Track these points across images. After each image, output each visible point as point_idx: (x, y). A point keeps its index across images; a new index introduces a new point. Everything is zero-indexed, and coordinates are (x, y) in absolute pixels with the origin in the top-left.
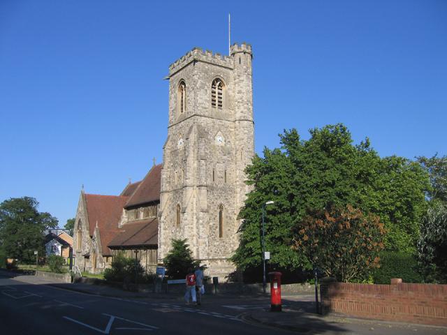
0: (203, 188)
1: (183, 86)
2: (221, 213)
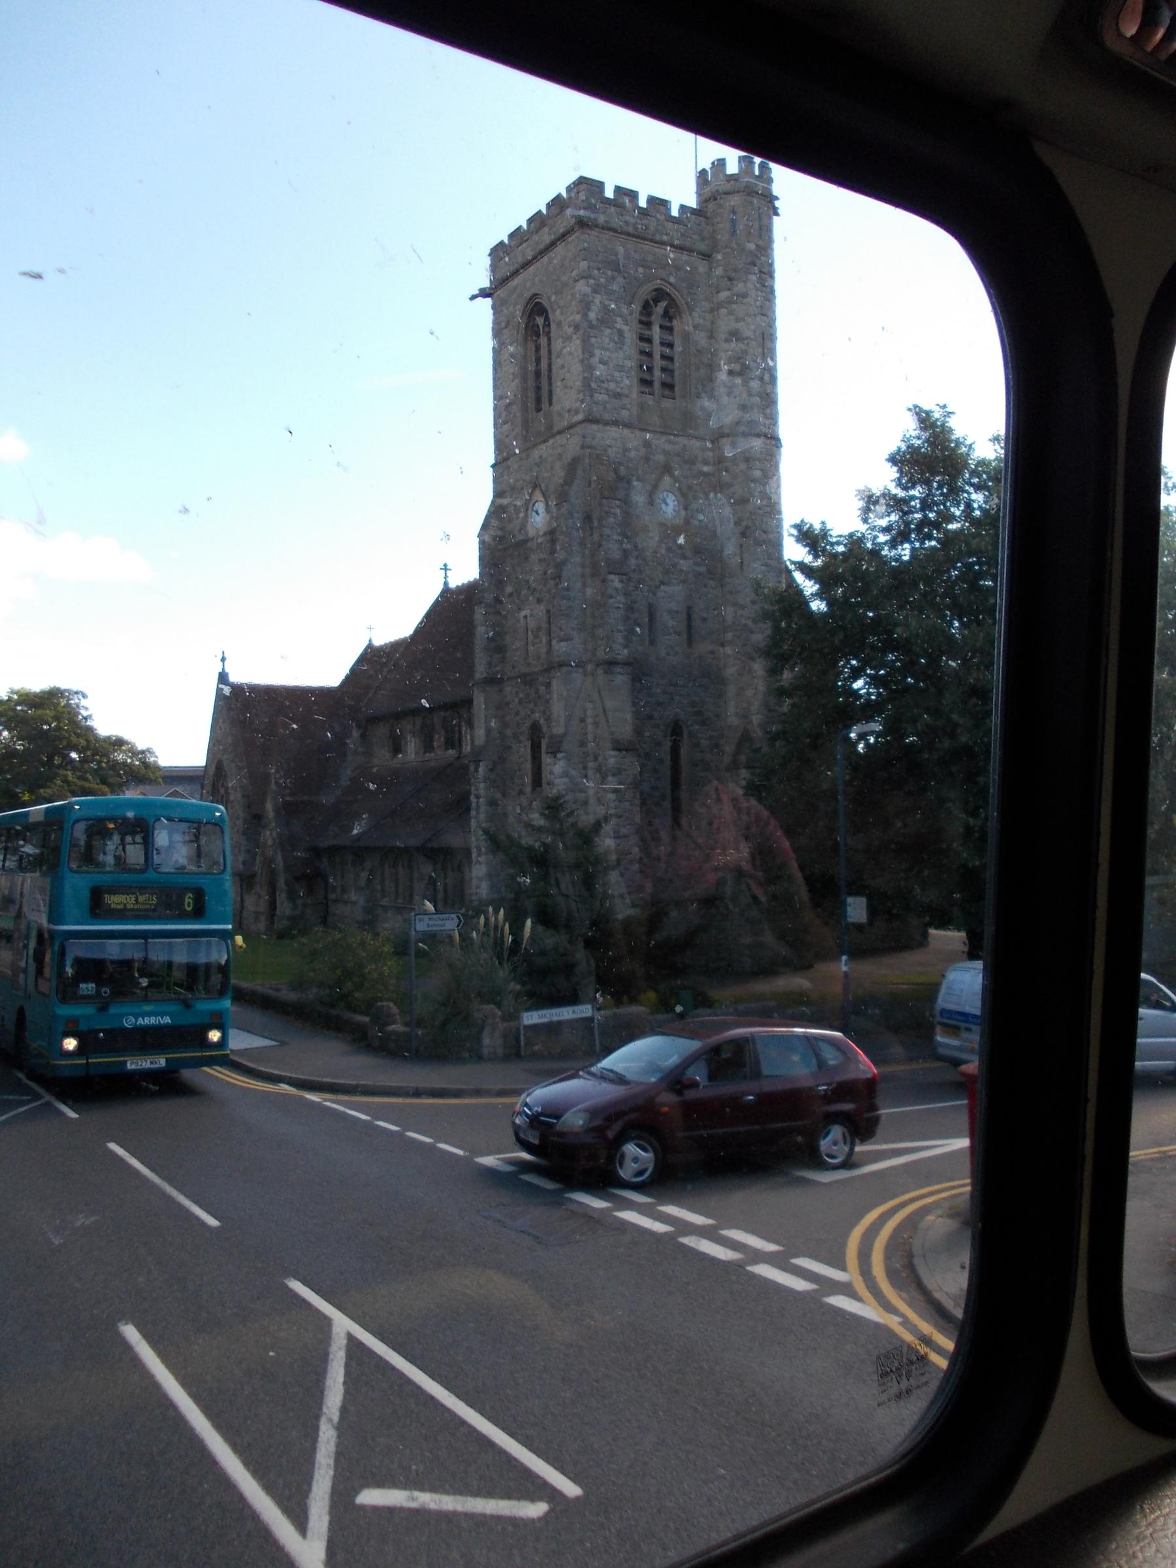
0: (618, 669)
1: (540, 321)
2: (675, 751)
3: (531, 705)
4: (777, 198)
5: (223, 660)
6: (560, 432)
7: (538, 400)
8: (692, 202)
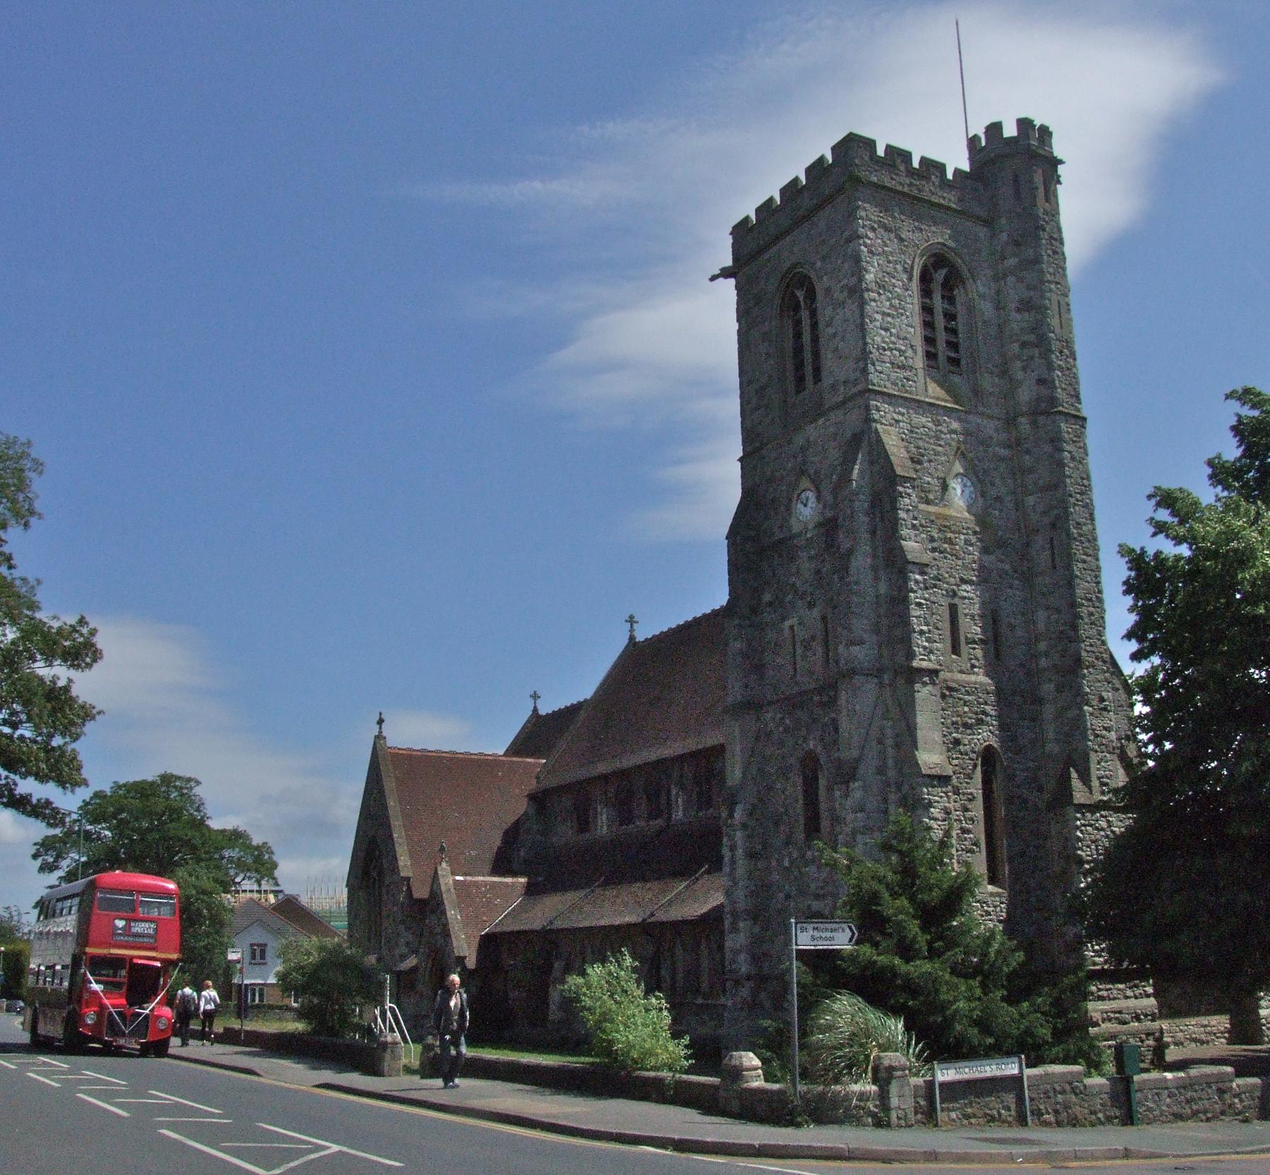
1: (800, 294)
3: (804, 732)
4: (1061, 162)
5: (381, 722)
6: (832, 409)
7: (800, 380)
8: (966, 167)
